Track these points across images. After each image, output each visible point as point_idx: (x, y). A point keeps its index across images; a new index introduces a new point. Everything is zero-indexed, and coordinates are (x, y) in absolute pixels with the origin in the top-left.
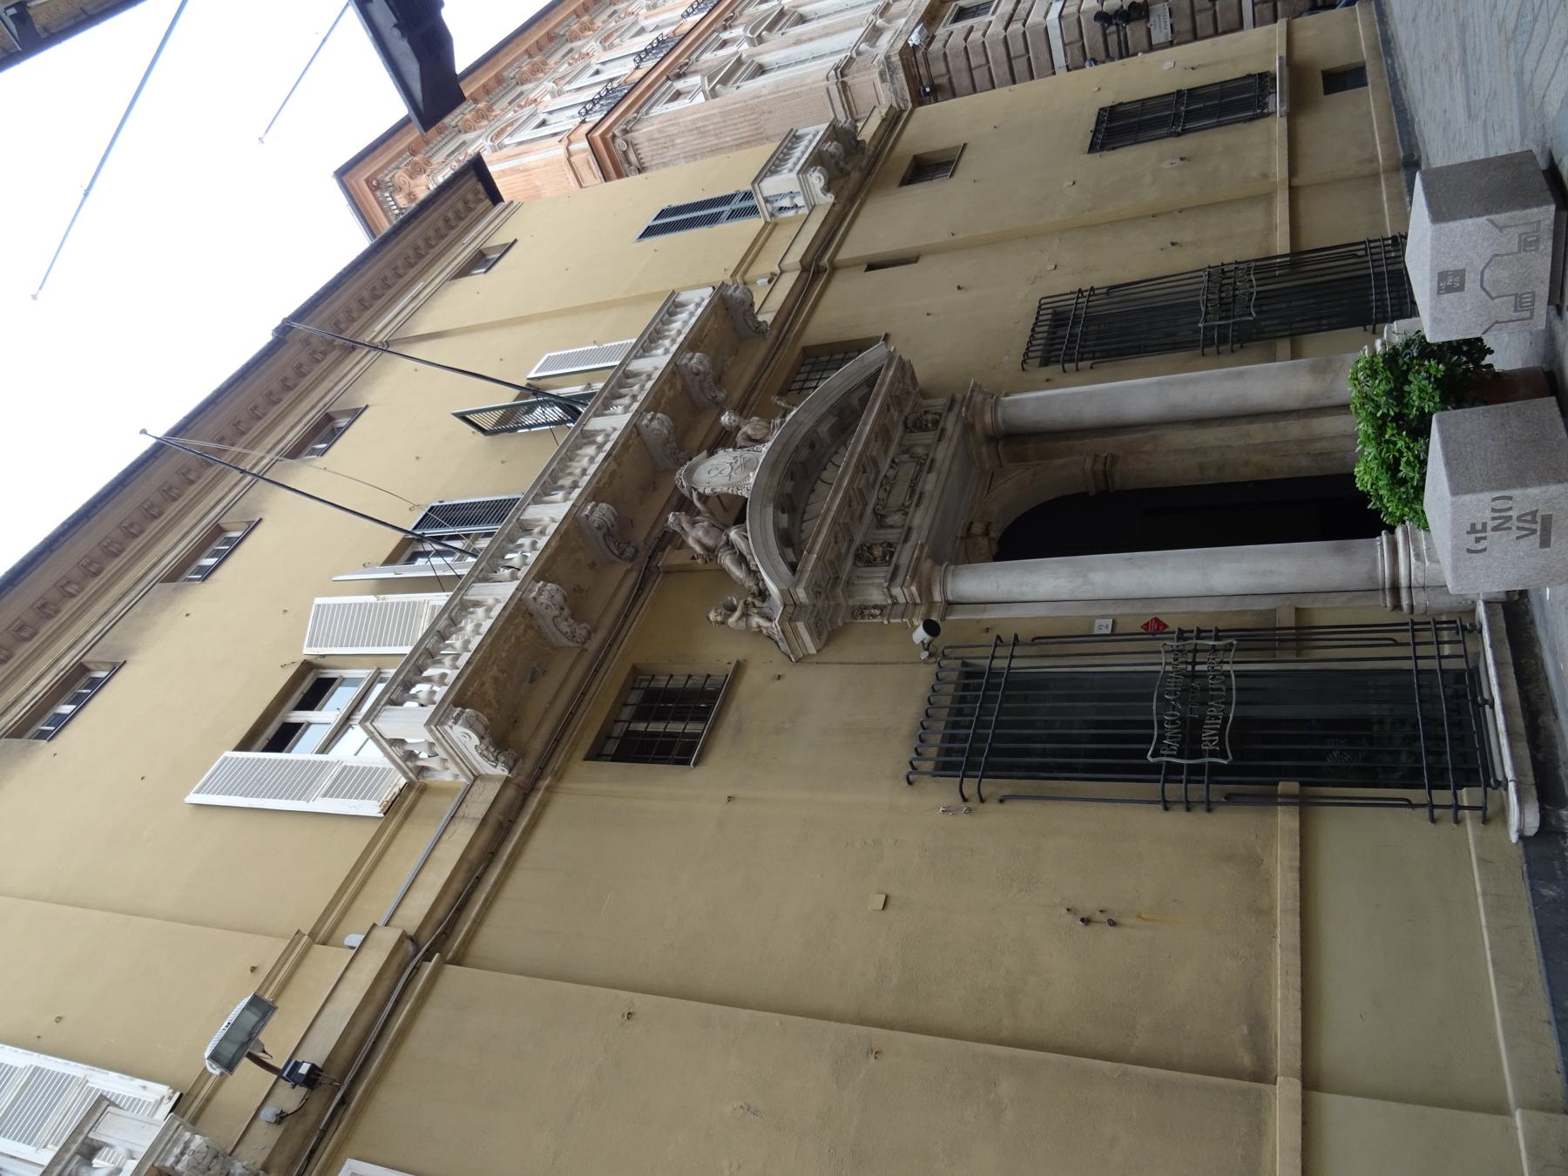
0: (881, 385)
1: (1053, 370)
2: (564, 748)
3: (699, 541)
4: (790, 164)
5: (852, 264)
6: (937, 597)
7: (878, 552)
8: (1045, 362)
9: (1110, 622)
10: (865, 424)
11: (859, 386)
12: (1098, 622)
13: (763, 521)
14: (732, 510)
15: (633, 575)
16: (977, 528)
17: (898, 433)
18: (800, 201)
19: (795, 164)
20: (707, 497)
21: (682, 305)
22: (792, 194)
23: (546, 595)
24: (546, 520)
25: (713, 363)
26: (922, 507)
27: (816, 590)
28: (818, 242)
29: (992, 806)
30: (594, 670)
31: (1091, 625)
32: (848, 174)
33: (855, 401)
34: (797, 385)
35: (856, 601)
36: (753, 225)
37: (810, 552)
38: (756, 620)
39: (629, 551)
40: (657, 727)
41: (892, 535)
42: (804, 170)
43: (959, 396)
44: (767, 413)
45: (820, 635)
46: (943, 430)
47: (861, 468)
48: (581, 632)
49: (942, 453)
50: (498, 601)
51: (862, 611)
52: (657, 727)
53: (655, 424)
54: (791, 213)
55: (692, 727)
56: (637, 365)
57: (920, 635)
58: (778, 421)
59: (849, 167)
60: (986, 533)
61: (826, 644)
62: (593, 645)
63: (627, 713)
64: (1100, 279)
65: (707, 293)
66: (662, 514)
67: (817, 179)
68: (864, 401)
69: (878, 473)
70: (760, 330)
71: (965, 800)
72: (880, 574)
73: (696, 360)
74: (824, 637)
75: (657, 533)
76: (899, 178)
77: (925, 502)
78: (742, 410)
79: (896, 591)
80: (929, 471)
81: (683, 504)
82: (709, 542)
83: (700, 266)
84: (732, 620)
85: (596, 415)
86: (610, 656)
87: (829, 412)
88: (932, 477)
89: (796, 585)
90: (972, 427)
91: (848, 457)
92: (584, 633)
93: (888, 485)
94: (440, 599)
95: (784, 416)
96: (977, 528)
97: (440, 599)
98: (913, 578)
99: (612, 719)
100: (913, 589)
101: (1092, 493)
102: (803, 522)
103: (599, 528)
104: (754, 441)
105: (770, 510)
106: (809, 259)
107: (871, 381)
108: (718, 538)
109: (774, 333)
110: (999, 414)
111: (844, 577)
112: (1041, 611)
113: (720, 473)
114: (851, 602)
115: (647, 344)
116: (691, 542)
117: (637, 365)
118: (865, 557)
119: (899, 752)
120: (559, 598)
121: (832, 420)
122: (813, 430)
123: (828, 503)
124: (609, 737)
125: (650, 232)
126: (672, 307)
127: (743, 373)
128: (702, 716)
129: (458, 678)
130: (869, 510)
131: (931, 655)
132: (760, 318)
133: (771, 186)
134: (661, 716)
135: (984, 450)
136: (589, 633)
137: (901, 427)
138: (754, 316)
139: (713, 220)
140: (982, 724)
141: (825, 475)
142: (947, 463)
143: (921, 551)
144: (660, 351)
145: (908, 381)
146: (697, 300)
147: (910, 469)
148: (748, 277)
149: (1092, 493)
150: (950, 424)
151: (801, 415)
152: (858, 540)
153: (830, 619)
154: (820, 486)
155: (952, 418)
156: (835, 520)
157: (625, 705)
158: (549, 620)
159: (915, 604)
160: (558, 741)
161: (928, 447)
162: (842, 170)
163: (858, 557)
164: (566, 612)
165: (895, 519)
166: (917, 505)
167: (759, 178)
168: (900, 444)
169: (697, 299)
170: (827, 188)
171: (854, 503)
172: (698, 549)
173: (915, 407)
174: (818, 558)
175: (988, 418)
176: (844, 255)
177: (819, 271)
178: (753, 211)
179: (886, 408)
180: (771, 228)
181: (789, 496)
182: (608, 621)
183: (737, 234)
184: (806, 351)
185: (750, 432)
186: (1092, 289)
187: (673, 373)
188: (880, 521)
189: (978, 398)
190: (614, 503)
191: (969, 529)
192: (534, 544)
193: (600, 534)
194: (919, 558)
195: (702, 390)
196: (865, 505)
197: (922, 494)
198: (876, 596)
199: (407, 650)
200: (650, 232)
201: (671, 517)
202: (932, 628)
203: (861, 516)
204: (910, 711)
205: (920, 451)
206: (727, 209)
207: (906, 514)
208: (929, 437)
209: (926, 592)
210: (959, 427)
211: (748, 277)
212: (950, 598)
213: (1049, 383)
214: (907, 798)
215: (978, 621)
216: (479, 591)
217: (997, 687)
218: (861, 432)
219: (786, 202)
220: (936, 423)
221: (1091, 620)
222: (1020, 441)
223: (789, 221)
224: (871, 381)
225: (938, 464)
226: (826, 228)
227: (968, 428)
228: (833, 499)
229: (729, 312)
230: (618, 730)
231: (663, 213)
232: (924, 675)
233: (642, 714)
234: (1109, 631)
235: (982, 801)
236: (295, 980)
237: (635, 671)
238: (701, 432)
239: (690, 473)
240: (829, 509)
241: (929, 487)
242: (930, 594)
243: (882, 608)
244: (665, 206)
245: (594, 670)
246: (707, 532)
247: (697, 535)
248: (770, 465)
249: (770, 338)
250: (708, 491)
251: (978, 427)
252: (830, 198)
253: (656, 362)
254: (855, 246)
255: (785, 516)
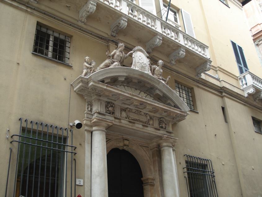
0: (173, 109)
1: (184, 165)
2: (42, 15)
3: (115, 54)
4: (256, 82)
5: (224, 102)
6: (94, 128)
7: (110, 109)
8: (187, 162)
9: (82, 184)
10: (158, 104)
11: (174, 102)
12: (82, 181)
13: (122, 73)
14: (126, 62)
15: (106, 36)
16: (126, 142)
17: (158, 115)
18: (245, 86)
19: (256, 84)
20: (132, 56)
21: (204, 50)
22: (246, 84)
23: (182, 53)
24: (121, 7)
25: (184, 58)
26: (128, 123)
27: (94, 88)
28: (232, 92)
29: (9, 145)
30: (71, 24)
31: (79, 178)
32: (255, 101)
33: (169, 102)
34: (180, 86)
35: (94, 103)
36: (237, 73)
37: (107, 86)
38: (85, 71)
39: (114, 34)
40: (51, 43)
41: (118, 114)
42: (253, 86)
43: (172, 135)
44: (164, 75)
45: (80, 91)
46: (159, 130)
47: (142, 103)
48: (84, 19)
49: (139, 126)
50: (206, 56)
51: (90, 104)
52: (51, 43)
53: (158, 40)
54: (241, 84)
55: (50, 54)
56: (181, 36)
57: (77, 122)
58: (161, 78)
59: (257, 101)
60: (125, 145)
61: (77, 94)
62: (80, 24)
63: (56, 35)
64: (218, 178)
65: (208, 57)
66: (122, 42)
67: (251, 91)
68: (169, 104)
69: (142, 109)
70: (199, 74)
71: (12, 137)
72: (103, 110)
73: (182, 53)
74: (79, 93)
75: (157, 59)
76: (254, 116)
77: (131, 124)
78: (164, 67)
79: (96, 115)
80: (143, 126)
81: (128, 49)
82: (115, 56)
83: (221, 57)
84: (86, 64)
85: (162, 24)
86: (76, 29)
87: (164, 94)
88: (141, 126)
89: (94, 82)
90: (161, 139)
91: (149, 100)
92: (83, 20)
93: (138, 112)
94: (155, 13)
95: (163, 80)
96: (126, 142)
97: (155, 13)
98: (99, 120)
99: (54, 30)
100: (95, 120)
101: (142, 179)
102: (124, 86)
103: (119, 23)
104: (153, 71)
105: (125, 74)
106: (225, 89)
107: (176, 106)
108: (116, 59)
109: (198, 79)
110: (166, 148)
111: (101, 98)
112: (87, 162)
113: (140, 59)
114: (93, 101)
115: (187, 38)
116: (115, 51)
117: (181, 36)
118: (108, 105)
119: (33, 115)
120: (91, 10)
121: (161, 95)
122: (157, 89)
123: (126, 92)
124: (47, 29)
125: (234, 44)
126: (203, 47)
127: (183, 69)
128: (54, 56)
129: (113, 8)
130: (127, 106)
131: (71, 126)
132: (202, 74)
133: (248, 77)
134: (55, 45)
135: (155, 144)
136: (83, 22)
137: (161, 116)
138: (202, 72)
139: (238, 62)
140: (50, 144)
141: (142, 93)
142: (147, 131)
143: (110, 122)
144: (186, 42)
145: (178, 119)
146: (206, 54)
147: (144, 119)
148: (218, 72)
149: (142, 179)
150: (161, 133)
151: (163, 84)
152: (115, 103)
153: (85, 93)
154: (138, 91)
155: (165, 133)
156: (120, 94)
157: (59, 34)
158: (85, 9)
159: (91, 121)
160: (45, 14)
161: (153, 125)
162: (256, 99)
163: (108, 103)
164: (88, 14)
165: (124, 114)
166: (129, 122)
167: (250, 73)
168: (154, 116)
169: (207, 54)
170: (249, 95)
171: (128, 101)
172: (113, 53)
173: (170, 121)
174: (105, 89)
175: (165, 144)
176: (227, 100)
177: (221, 93)
178: (241, 72)
179: (166, 111)
180: (236, 78)
181: (132, 81)
182: (89, 28)
183: (234, 69)
184: (192, 89)
185: (156, 69)
186: (214, 176)
187: (179, 46)
188: (123, 110)
189: (171, 140)
190: (186, 56)
191: (126, 140)
192: (145, 21)
193: (118, 24)
194: (107, 122)
195: (174, 56)
196: (129, 105)
197: (134, 123)
198: (95, 109)
199: (140, 6)
200: (234, 44)
201: (121, 44)
202: (79, 126)
203: (125, 104)
204: (48, 119)
205: (151, 122)
206: (243, 66)
207: (126, 118)
208: (156, 125)
209: (95, 124)
210: (160, 135)
211: (218, 72)
212: (94, 133)
213: (179, 163)
214: (14, 118)
215: (84, 142)
216: (158, 23)
217: (59, 148)
218: (155, 103)
219: (244, 82)
220: (162, 127)
221: (83, 178)
222: (158, 154)
223: (239, 84)
224: (176, 106)
225: (145, 128)
226: (236, 94)
227: (161, 138)
228: (128, 93)
229: (202, 64)
230: (50, 32)
231: (240, 48)
232: (64, 125)
233: (56, 39)
234: (77, 183)
235: (184, 172)
236: (225, 75)
237: (71, 37)
238: (156, 54)
239: (140, 51)
240: (124, 92)
241: (137, 125)
242: (95, 126)
243: (91, 110)
244: (243, 49)
245: (71, 24)
246: (118, 56)
247: (117, 52)
248: (142, 75)
249: (196, 78)
250: (133, 56)
251: (161, 141)
252: (246, 95)
253: (181, 41)
254: (230, 104)
255: (124, 79)
